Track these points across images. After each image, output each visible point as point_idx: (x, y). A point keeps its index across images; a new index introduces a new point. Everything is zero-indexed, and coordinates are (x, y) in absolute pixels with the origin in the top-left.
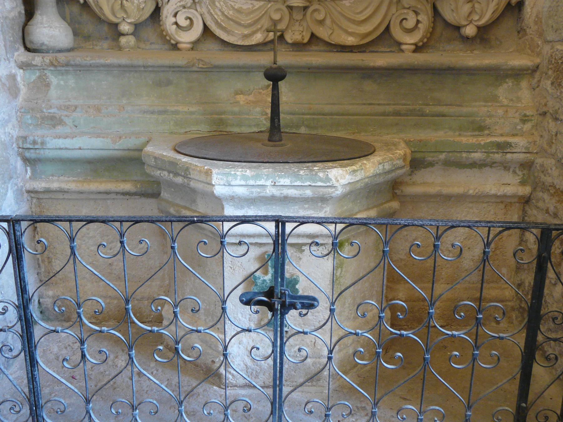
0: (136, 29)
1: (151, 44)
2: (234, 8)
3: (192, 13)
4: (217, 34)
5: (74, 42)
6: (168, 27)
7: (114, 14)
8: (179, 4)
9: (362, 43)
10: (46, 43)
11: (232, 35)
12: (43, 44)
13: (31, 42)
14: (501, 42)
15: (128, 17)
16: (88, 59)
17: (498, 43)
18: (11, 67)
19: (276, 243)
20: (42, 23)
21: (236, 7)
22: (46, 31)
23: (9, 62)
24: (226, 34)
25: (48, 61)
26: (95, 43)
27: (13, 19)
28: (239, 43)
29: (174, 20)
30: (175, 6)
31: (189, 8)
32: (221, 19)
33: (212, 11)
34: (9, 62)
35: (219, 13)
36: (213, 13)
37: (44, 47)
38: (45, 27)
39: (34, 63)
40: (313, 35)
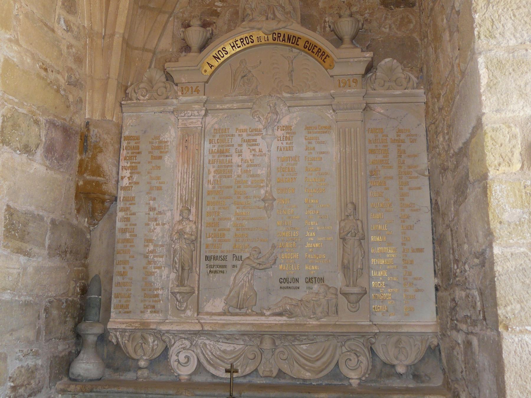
0: (151, 364)
1: (161, 375)
2: (220, 350)
3: (189, 353)
4: (208, 369)
5: (73, 360)
6: (172, 363)
7: (135, 352)
8: (181, 347)
9: (317, 377)
10: (82, 374)
11: (218, 370)
12: (79, 375)
13: (73, 374)
14: (430, 378)
15: (144, 355)
16: (106, 387)
17: (428, 379)
18: (52, 393)
19: (26, 251)
20: (82, 360)
21: (222, 349)
22: (83, 365)
23: (50, 389)
24: (214, 369)
25: (79, 388)
26: (121, 374)
27: (63, 357)
28: (223, 377)
29: (176, 358)
30: (178, 348)
31: (188, 349)
32: (210, 358)
33: (204, 352)
34: (50, 389)
35: (210, 354)
36: (205, 353)
37: (80, 378)
38: (83, 363)
39: (69, 390)
40: (280, 370)
